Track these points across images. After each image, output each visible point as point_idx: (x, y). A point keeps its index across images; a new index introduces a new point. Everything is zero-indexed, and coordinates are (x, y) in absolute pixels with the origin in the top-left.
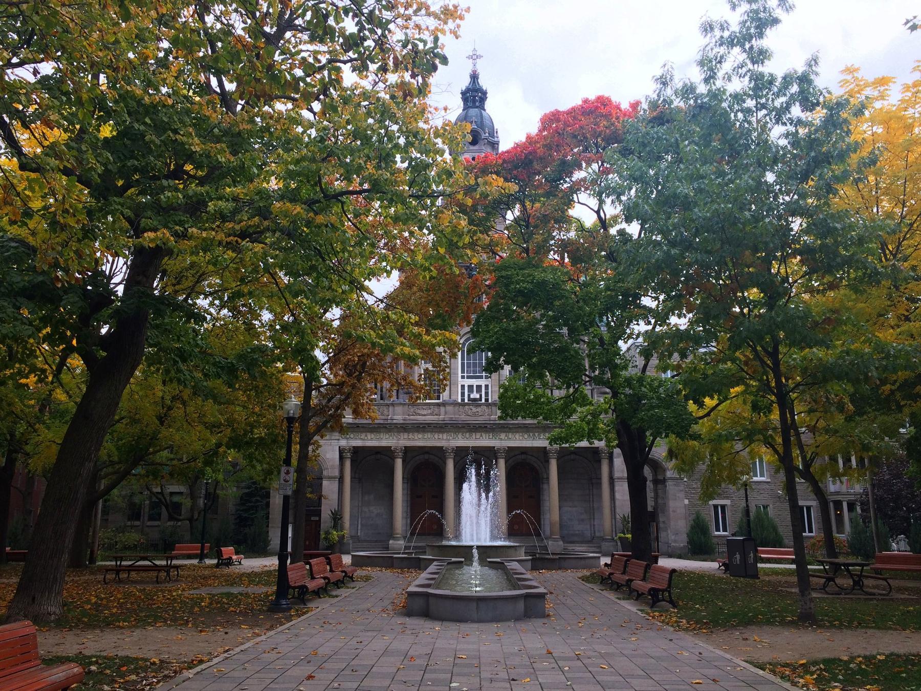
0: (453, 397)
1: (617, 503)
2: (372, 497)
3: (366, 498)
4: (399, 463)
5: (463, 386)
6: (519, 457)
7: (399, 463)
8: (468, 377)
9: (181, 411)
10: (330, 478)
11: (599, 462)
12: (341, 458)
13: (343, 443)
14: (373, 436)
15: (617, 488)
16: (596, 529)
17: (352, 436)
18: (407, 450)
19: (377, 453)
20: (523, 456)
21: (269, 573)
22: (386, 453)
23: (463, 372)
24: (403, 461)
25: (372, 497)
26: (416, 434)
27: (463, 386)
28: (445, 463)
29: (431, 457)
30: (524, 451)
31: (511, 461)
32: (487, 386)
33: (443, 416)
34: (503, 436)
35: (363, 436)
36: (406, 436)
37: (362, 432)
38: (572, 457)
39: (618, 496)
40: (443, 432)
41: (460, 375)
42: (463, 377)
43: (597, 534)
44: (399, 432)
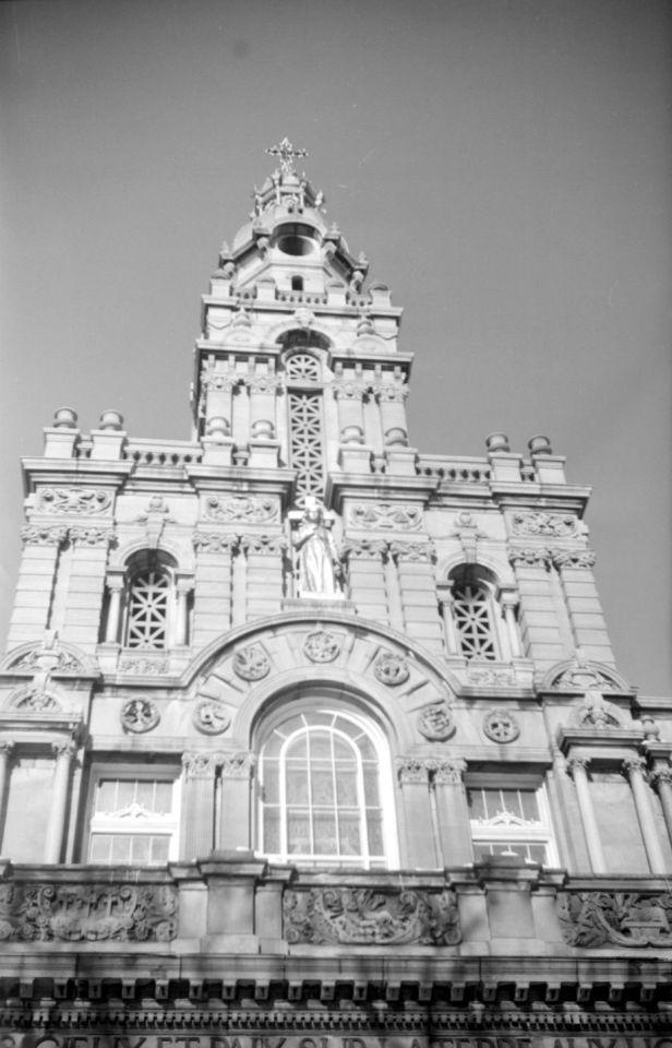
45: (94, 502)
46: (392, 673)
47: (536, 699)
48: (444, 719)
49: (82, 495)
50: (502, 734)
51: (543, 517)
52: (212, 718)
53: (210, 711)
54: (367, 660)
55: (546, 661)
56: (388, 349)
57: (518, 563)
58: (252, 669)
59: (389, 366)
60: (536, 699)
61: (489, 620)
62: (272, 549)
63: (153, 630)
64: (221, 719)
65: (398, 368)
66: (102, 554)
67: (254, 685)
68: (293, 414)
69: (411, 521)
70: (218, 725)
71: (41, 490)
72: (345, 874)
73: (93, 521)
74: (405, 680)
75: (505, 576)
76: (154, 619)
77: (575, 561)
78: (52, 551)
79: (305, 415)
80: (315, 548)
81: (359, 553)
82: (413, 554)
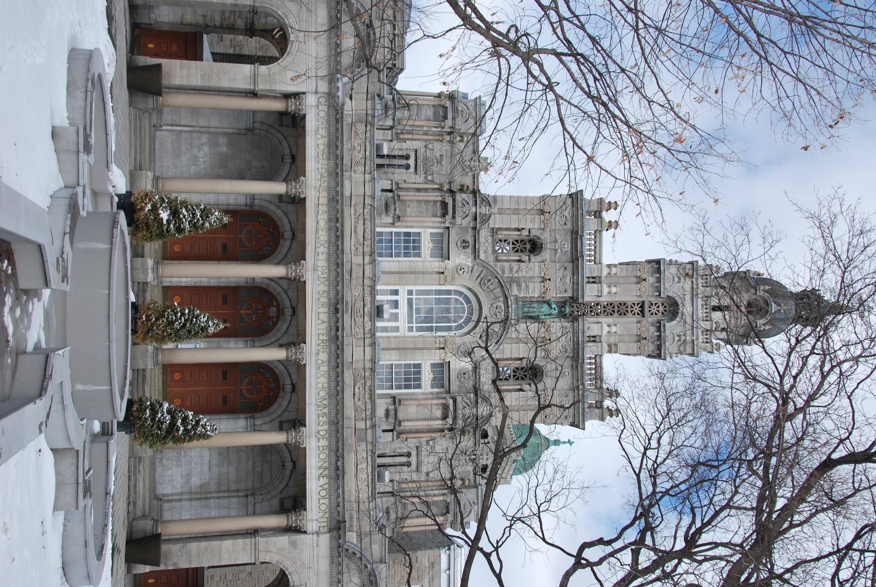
0: (383, 278)
1: (215, 543)
2: (224, 149)
3: (222, 140)
4: (278, 188)
5: (396, 292)
6: (288, 382)
7: (278, 188)
8: (410, 302)
9: (813, 343)
10: (255, 77)
11: (283, 510)
12: (287, 96)
13: (311, 100)
14: (321, 147)
15: (240, 541)
16: (174, 504)
17: (322, 114)
18: (298, 202)
19: (293, 158)
20: (288, 388)
21: (134, 458)
22: (291, 164)
23: (419, 292)
24: (280, 196)
25: (224, 149)
26: (325, 217)
27: (396, 292)
28: (278, 263)
29: (287, 244)
30: (298, 388)
31: (282, 368)
32: (397, 329)
33: (354, 259)
34: (324, 356)
35: (323, 132)
36: (324, 201)
37: (328, 129)
38: (289, 465)
39: (227, 543)
40: (328, 260)
41: (414, 288)
42: (410, 292)
43: (166, 506)
44: (329, 189)
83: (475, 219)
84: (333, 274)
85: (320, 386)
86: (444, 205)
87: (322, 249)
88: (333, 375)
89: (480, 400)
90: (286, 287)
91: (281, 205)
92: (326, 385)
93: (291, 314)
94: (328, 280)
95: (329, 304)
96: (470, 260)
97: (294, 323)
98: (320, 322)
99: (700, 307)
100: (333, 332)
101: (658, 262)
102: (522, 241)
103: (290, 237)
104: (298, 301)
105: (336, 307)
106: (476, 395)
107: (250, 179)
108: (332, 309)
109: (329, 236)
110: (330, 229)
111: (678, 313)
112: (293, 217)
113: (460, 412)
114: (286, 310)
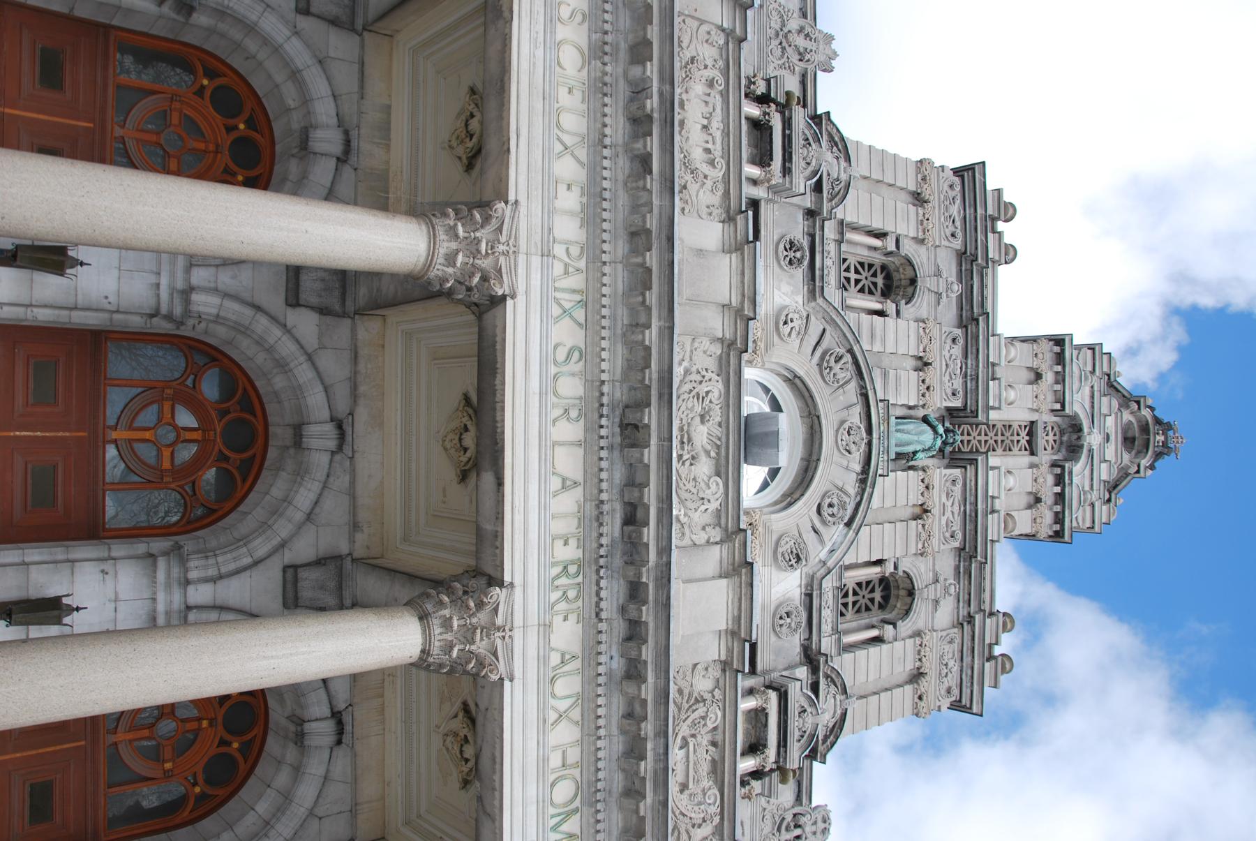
34: (567, 634)
40: (592, 217)
45: (951, 229)
46: (830, 510)
47: (811, 658)
48: (793, 561)
49: (957, 219)
50: (782, 622)
51: (954, 666)
52: (791, 325)
53: (796, 324)
54: (840, 485)
55: (846, 665)
56: (1078, 516)
57: (918, 641)
58: (831, 368)
59: (1059, 519)
60: (811, 658)
61: (864, 614)
62: (923, 395)
63: (857, 272)
64: (789, 335)
65: (1057, 527)
66: (912, 234)
67: (816, 368)
68: (1015, 426)
69: (948, 535)
70: (786, 329)
71: (957, 180)
72: (728, 406)
73: (939, 228)
74: (824, 522)
75: (905, 627)
76: (857, 282)
77: (920, 698)
78: (912, 187)
79: (999, 438)
80: (927, 437)
81: (922, 481)
82: (924, 536)
83: (818, 188)
84: (616, 278)
85: (555, 760)
86: (760, 128)
87: (569, 169)
88: (612, 708)
89: (822, 682)
90: (311, 341)
91: (304, 23)
92: (574, 755)
93: (332, 444)
94: (590, 301)
95: (593, 407)
96: (800, 299)
97: (341, 481)
98: (555, 483)
99: (654, 426)
100: (613, 527)
101: (1059, 341)
102: (871, 266)
103: (337, 148)
104: (354, 395)
105: (630, 422)
106: (815, 670)
107: (27, 150)
108: (609, 428)
109: (597, 118)
110: (598, 88)
111: (1082, 447)
112: (346, 79)
113: (794, 723)
114: (312, 429)
